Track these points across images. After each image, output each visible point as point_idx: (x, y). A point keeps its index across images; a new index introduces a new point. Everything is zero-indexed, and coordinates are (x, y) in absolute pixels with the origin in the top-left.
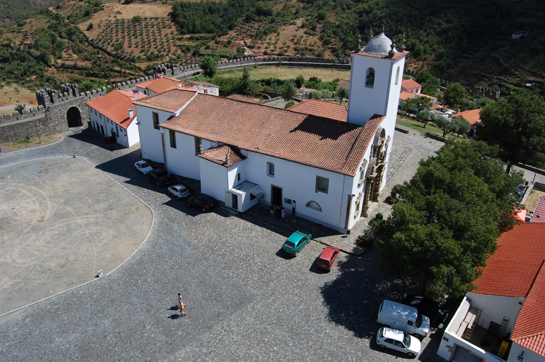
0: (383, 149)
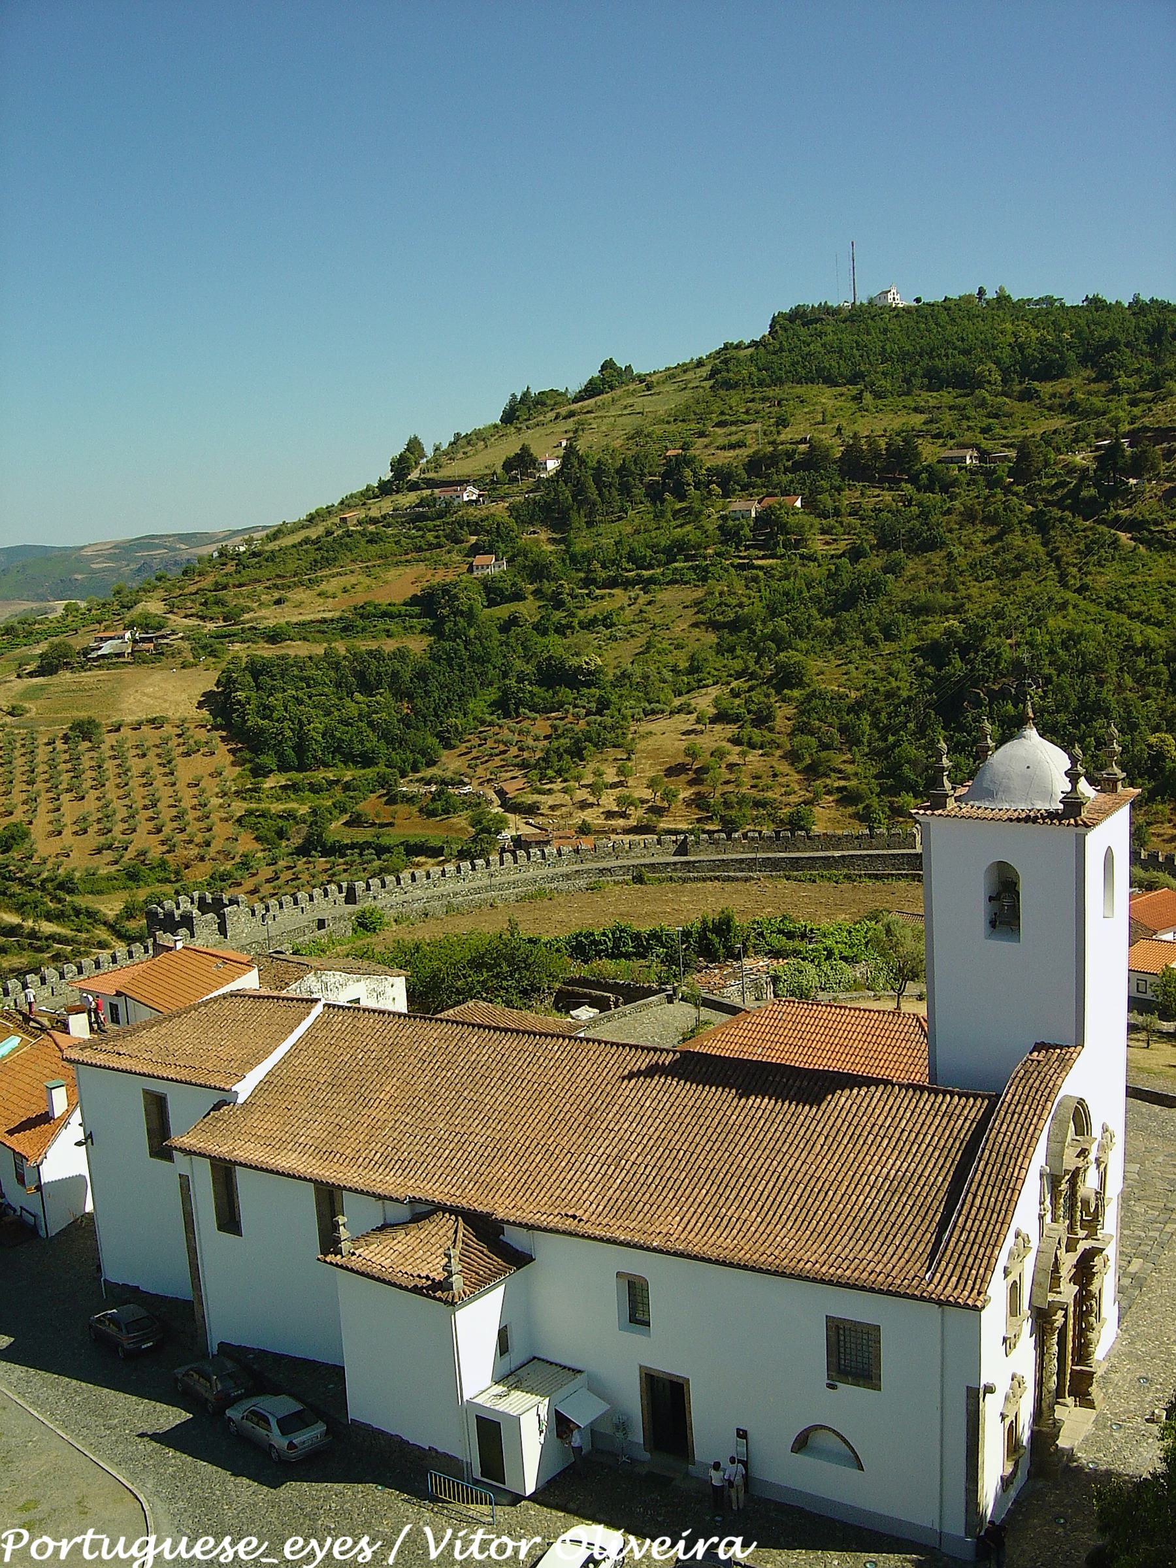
0: (1090, 1183)
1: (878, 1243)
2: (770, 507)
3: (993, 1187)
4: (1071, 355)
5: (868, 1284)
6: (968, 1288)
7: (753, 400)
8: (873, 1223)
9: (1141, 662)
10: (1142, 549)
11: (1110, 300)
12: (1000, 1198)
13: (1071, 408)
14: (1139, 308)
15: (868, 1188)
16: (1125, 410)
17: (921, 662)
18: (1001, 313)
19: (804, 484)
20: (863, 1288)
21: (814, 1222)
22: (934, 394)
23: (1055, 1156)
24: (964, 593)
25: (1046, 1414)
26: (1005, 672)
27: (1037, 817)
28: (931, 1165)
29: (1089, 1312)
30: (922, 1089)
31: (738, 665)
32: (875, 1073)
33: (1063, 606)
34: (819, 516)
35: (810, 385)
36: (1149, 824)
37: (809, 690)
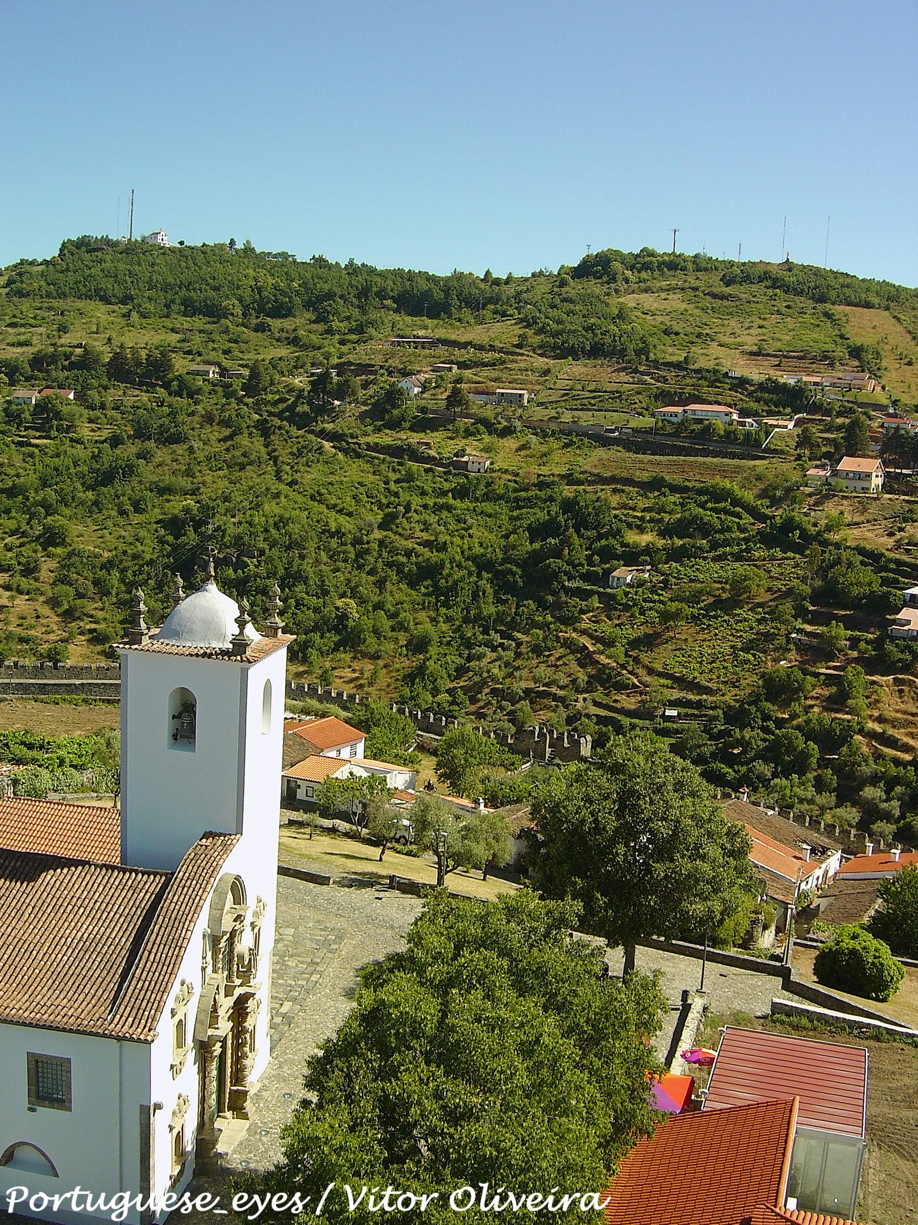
0: (244, 945)
1: (71, 992)
2: (47, 397)
3: (165, 945)
4: (297, 300)
5: (61, 1025)
6: (142, 1026)
7: (40, 309)
8: (68, 976)
9: (334, 543)
10: (340, 456)
11: (332, 261)
12: (170, 954)
13: (294, 341)
14: (353, 269)
15: (65, 948)
16: (334, 347)
17: (162, 532)
18: (246, 261)
19: (77, 381)
20: (57, 1029)
21: (20, 976)
22: (188, 319)
23: (216, 920)
24: (200, 479)
25: (207, 1125)
26: (228, 544)
27: (212, 654)
28: (117, 929)
29: (244, 1044)
30: (113, 868)
31: (12, 525)
32: (84, 856)
33: (277, 495)
34: (88, 407)
35: (88, 301)
36: (333, 669)
37: (70, 549)
